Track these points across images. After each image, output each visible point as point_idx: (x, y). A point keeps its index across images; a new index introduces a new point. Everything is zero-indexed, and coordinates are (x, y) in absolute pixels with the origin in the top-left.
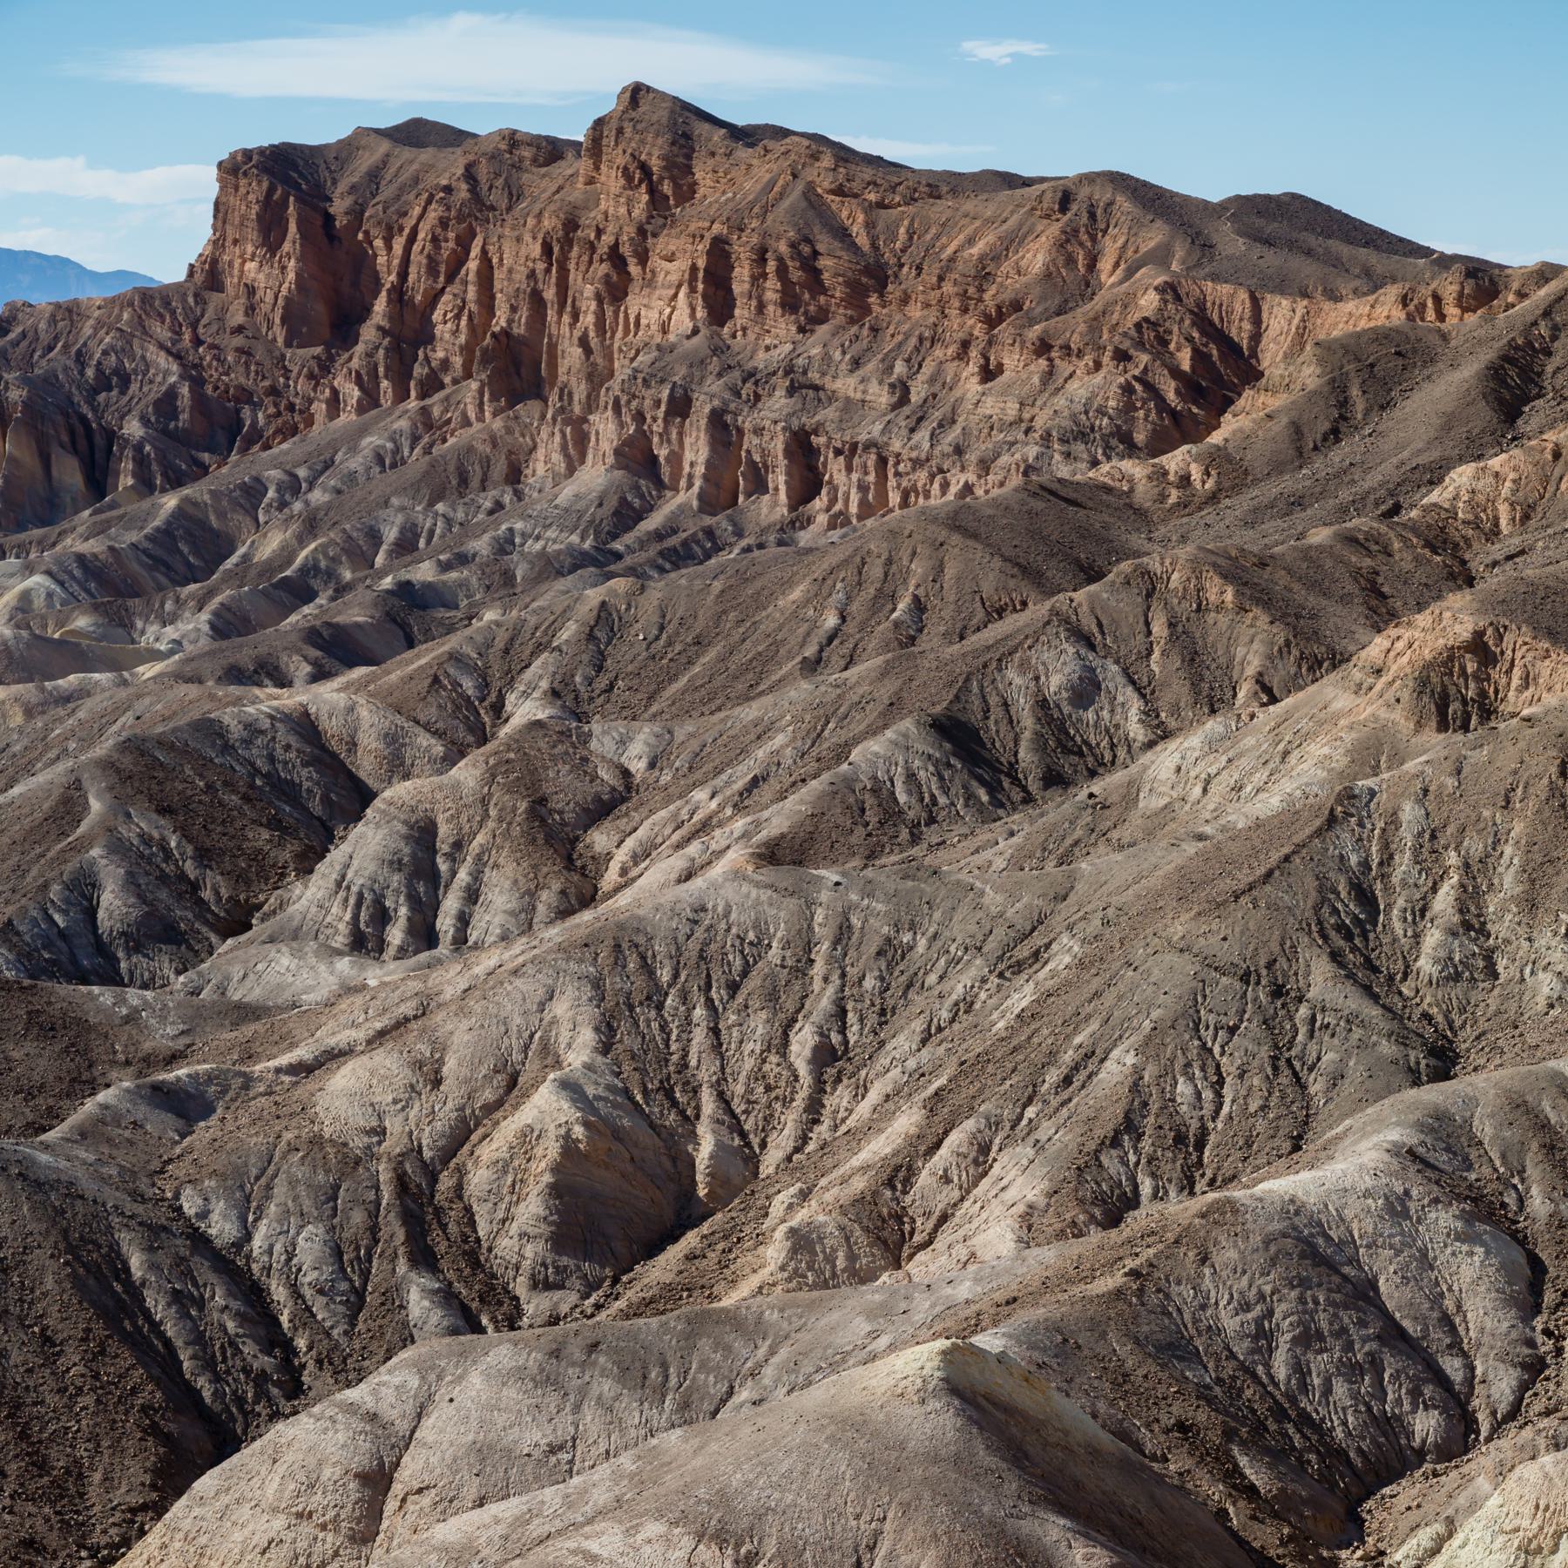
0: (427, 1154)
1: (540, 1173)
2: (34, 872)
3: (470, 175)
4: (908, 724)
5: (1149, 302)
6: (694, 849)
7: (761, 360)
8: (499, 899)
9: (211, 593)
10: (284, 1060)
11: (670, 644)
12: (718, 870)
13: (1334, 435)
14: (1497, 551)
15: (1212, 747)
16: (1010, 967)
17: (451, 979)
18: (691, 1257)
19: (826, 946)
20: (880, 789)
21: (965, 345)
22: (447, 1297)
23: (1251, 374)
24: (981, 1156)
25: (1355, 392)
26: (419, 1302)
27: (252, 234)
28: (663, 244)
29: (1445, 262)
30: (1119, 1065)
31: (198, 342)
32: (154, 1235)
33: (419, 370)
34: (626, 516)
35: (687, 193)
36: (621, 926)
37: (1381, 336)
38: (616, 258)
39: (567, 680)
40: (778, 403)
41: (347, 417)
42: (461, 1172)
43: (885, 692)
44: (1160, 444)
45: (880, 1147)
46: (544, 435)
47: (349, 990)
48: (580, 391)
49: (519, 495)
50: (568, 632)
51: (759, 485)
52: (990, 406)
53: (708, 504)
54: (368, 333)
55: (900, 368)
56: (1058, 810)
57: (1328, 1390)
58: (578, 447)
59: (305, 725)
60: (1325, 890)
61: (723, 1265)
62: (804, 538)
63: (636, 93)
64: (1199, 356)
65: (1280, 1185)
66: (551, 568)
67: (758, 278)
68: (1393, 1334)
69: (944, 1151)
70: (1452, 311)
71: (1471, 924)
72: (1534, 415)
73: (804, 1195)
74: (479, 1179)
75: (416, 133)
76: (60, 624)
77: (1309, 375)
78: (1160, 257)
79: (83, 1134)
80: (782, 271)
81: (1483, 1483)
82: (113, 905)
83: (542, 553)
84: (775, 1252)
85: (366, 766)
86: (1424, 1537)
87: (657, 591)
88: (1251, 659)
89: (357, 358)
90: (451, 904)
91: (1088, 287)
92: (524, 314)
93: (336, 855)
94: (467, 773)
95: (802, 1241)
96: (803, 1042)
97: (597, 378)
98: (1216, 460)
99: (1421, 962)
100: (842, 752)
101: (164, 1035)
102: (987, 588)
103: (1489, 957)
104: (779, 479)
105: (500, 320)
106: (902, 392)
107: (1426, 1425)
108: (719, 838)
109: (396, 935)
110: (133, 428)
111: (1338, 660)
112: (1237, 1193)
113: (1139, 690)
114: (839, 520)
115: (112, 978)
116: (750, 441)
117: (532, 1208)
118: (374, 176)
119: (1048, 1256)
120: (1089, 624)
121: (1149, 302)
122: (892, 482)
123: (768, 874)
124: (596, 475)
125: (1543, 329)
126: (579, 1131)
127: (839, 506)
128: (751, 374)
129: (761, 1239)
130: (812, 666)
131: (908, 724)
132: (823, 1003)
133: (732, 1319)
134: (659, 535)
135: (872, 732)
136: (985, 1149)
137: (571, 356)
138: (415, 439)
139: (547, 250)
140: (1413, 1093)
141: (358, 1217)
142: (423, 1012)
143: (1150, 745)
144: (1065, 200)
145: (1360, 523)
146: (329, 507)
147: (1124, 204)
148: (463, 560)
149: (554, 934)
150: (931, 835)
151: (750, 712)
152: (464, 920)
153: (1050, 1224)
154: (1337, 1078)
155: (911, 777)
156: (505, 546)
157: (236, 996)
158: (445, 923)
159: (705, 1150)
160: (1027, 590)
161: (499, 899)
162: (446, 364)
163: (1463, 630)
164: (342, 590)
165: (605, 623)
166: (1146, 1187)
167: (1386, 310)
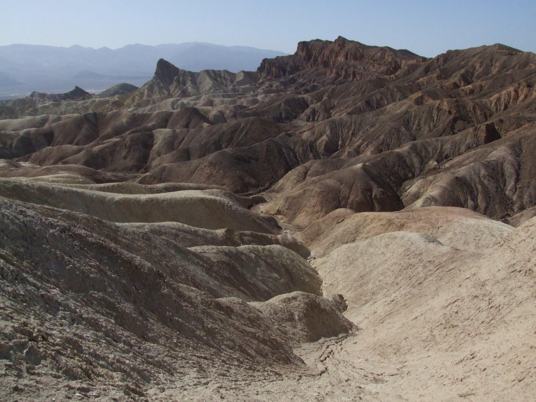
3: (323, 45)
4: (363, 101)
5: (390, 60)
6: (341, 113)
7: (350, 64)
8: (321, 116)
10: (300, 131)
12: (343, 115)
13: (408, 74)
14: (424, 87)
15: (394, 105)
16: (372, 126)
20: (360, 108)
21: (371, 63)
22: (314, 156)
23: (400, 68)
24: (367, 146)
26: (311, 156)
28: (342, 52)
29: (421, 57)
30: (382, 137)
32: (286, 148)
33: (316, 64)
34: (336, 79)
35: (344, 46)
37: (414, 64)
40: (352, 69)
41: (309, 68)
42: (316, 144)
44: (390, 75)
45: (357, 144)
47: (306, 125)
48: (332, 67)
50: (329, 91)
51: (349, 77)
52: (373, 70)
53: (344, 78)
54: (312, 60)
56: (378, 111)
57: (400, 171)
58: (331, 72)
59: (303, 98)
60: (404, 121)
61: (341, 154)
64: (395, 66)
65: (397, 150)
67: (351, 56)
68: (407, 166)
70: (421, 62)
71: (419, 125)
72: (429, 73)
73: (350, 148)
74: (318, 144)
77: (406, 68)
78: (392, 55)
79: (280, 138)
80: (353, 55)
81: (415, 181)
82: (283, 115)
84: (346, 153)
85: (309, 102)
86: (409, 186)
87: (339, 87)
89: (310, 62)
90: (316, 117)
91: (384, 58)
93: (305, 111)
94: (319, 104)
96: (351, 132)
97: (334, 65)
98: (396, 76)
100: (356, 104)
101: (288, 128)
103: (420, 129)
104: (352, 76)
105: (325, 59)
106: (364, 68)
107: (410, 175)
108: (343, 112)
109: (311, 120)
110: (288, 69)
111: (407, 97)
112: (393, 151)
113: (386, 99)
114: (357, 80)
115: (283, 123)
116: (349, 72)
117: (323, 147)
118: (313, 44)
119: (373, 156)
120: (382, 92)
121: (390, 60)
123: (348, 116)
124: (333, 75)
125: (431, 64)
129: (345, 152)
131: (363, 101)
132: (353, 128)
133: (342, 160)
134: (339, 81)
136: (368, 144)
137: (331, 63)
139: (330, 52)
141: (306, 147)
142: (313, 127)
143: (387, 105)
145: (411, 83)
147: (388, 50)
148: (320, 83)
149: (327, 120)
150: (364, 113)
151: (347, 99)
154: (404, 140)
155: (363, 106)
156: (324, 81)
158: (316, 119)
159: (340, 143)
161: (321, 116)
162: (319, 63)
163: (420, 95)
164: (307, 85)
165: (333, 90)
166: (384, 149)
167: (414, 61)
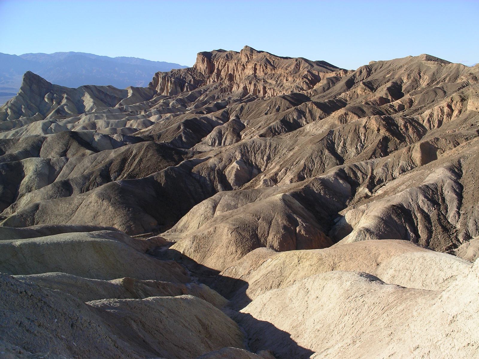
0: (221, 169)
1: (234, 172)
2: (175, 135)
4: (278, 121)
5: (306, 73)
6: (252, 135)
9: (195, 103)
11: (249, 111)
13: (328, 89)
17: (223, 149)
18: (251, 183)
19: (268, 147)
25: (331, 84)
27: (201, 62)
29: (341, 69)
30: (302, 162)
31: (194, 74)
35: (252, 58)
36: (244, 143)
38: (243, 65)
39: (237, 115)
43: (275, 117)
46: (234, 86)
49: (231, 93)
52: (287, 84)
54: (214, 73)
55: (276, 79)
62: (265, 99)
63: (246, 46)
66: (235, 101)
69: (282, 171)
75: (220, 51)
76: (177, 106)
78: (307, 67)
83: (234, 100)
84: (261, 183)
88: (318, 115)
92: (232, 71)
94: (225, 125)
95: (265, 181)
96: (265, 158)
99: (339, 151)
102: (287, 105)
119: (294, 184)
122: (275, 92)
126: (239, 168)
127: (269, 95)
128: (259, 79)
129: (260, 181)
130: (266, 114)
133: (257, 190)
134: (247, 98)
135: (273, 122)
137: (238, 76)
138: (219, 86)
139: (235, 64)
140: (338, 166)
144: (296, 60)
146: (209, 94)
151: (259, 119)
152: (225, 142)
153: (294, 180)
155: (278, 127)
156: (230, 98)
157: (198, 150)
160: (291, 106)
164: (210, 103)
165: (242, 108)
